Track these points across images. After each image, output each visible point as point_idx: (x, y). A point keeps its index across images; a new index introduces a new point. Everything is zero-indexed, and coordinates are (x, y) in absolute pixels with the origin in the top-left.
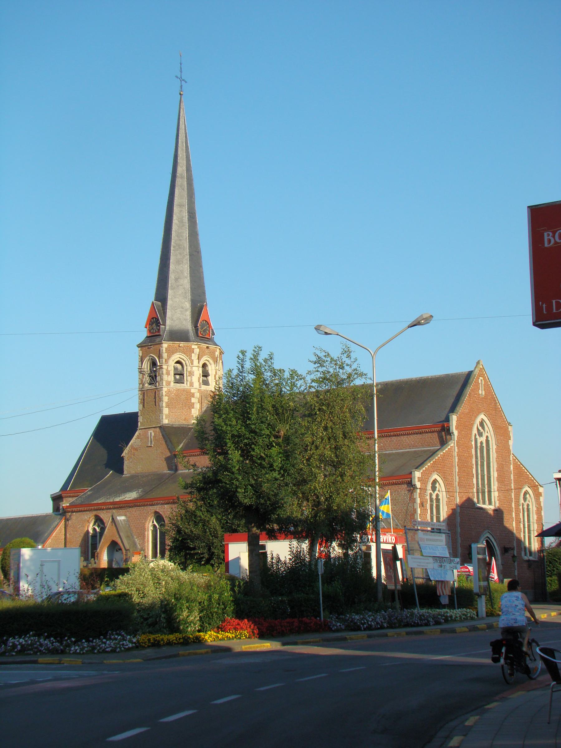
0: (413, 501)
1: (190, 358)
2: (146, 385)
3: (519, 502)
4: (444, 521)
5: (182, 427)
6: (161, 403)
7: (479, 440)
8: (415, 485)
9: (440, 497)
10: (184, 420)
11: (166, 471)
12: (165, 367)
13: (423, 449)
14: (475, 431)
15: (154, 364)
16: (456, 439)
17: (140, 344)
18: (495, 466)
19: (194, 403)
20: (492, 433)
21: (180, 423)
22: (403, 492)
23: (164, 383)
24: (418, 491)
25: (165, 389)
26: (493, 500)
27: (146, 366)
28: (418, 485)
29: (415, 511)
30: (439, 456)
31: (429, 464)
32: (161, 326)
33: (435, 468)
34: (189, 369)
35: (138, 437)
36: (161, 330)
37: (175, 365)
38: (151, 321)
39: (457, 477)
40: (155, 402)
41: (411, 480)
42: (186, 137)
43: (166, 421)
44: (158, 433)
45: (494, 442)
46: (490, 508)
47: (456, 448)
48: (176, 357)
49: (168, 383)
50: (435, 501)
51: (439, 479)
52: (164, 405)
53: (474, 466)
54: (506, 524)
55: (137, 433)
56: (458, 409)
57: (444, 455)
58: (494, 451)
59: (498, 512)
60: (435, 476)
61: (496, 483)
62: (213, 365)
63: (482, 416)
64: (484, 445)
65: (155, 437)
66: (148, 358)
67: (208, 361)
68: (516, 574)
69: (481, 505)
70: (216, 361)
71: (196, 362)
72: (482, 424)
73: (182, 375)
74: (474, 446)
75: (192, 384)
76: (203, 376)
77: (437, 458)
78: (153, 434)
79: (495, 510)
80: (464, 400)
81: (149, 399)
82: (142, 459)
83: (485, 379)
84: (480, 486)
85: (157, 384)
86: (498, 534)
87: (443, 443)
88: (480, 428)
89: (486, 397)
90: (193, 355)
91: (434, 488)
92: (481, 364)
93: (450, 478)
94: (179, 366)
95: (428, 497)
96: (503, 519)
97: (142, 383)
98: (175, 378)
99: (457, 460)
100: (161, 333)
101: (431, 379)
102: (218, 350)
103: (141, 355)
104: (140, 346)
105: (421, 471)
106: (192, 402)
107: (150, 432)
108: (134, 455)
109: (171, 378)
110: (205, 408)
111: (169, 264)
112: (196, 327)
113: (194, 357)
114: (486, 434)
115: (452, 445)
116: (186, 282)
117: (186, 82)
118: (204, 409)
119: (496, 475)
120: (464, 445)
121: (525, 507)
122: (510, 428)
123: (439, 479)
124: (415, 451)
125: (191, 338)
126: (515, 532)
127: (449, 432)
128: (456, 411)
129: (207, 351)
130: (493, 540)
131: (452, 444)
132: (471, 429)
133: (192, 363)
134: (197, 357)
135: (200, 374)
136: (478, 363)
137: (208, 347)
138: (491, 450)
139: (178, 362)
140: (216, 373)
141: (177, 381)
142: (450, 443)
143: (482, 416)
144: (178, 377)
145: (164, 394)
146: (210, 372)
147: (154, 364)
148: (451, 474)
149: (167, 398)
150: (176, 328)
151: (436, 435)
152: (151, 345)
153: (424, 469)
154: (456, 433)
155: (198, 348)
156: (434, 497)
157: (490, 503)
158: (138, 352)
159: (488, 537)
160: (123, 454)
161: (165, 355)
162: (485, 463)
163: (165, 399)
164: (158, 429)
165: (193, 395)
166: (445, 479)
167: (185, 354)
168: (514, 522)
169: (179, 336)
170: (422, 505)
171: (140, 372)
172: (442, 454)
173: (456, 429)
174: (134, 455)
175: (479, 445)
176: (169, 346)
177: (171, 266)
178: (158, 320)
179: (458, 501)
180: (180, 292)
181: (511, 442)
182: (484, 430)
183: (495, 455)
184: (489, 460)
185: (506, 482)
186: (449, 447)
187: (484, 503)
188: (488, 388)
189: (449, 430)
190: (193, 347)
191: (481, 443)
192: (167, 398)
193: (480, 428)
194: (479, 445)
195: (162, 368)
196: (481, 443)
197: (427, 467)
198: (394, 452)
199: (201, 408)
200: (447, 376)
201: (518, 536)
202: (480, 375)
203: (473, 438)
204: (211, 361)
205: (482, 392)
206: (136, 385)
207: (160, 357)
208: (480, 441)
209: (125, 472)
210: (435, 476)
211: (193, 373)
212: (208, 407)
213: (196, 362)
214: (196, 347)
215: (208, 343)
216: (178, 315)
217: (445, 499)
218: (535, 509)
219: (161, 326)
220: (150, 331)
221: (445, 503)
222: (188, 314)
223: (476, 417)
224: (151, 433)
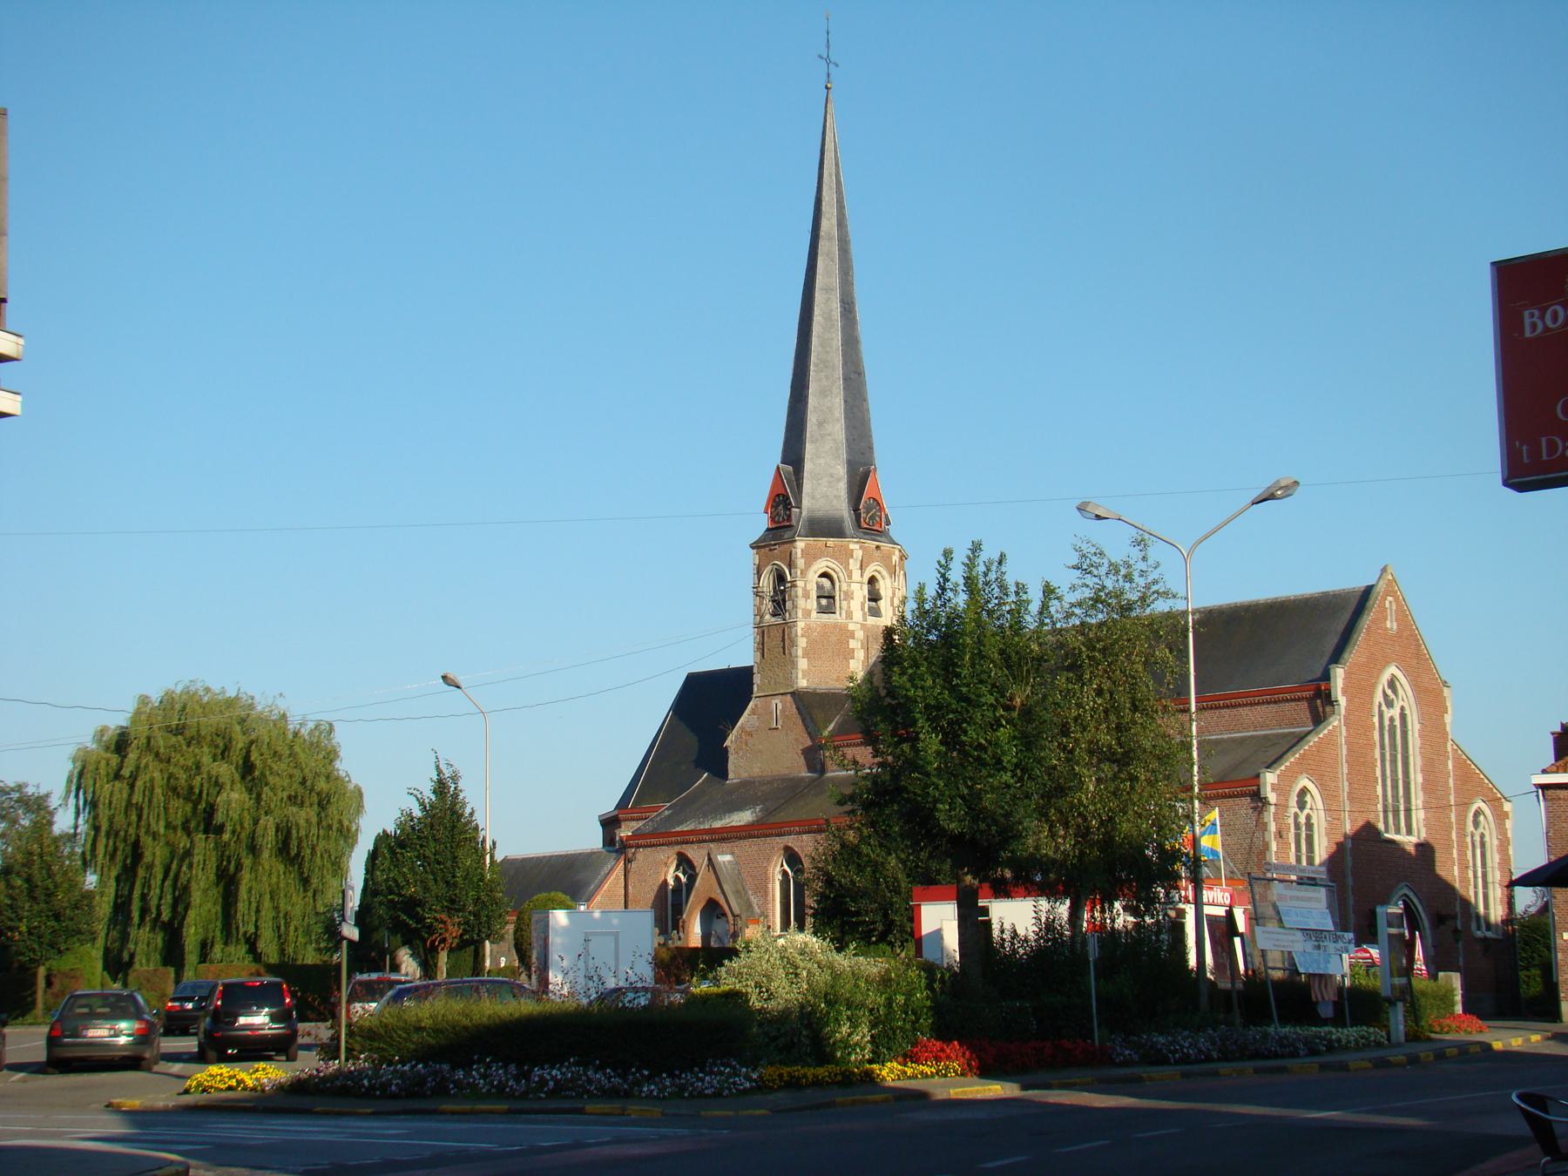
0: (1263, 827)
1: (847, 566)
2: (767, 617)
7: (1388, 713)
11: (805, 774)
14: (1379, 698)
15: (780, 578)
16: (1343, 712)
24: (1272, 809)
25: (801, 625)
28: (1272, 797)
29: (1266, 846)
34: (844, 587)
35: (753, 712)
43: (803, 683)
46: (1408, 841)
48: (821, 565)
49: (807, 613)
51: (1311, 786)
52: (800, 652)
54: (1441, 871)
56: (1346, 655)
59: (1426, 850)
60: (1305, 782)
61: (1421, 794)
62: (888, 580)
63: (1392, 670)
64: (1397, 723)
65: (783, 711)
71: (856, 575)
72: (1392, 684)
75: (849, 615)
81: (773, 642)
87: (1318, 719)
88: (1389, 692)
89: (1399, 635)
91: (1302, 805)
95: (1291, 821)
97: (759, 614)
99: (1345, 752)
100: (794, 522)
109: (812, 604)
112: (856, 510)
113: (854, 565)
118: (872, 660)
119: (1420, 779)
121: (1477, 838)
123: (1311, 786)
126: (1457, 885)
127: (1329, 700)
129: (877, 553)
131: (1336, 723)
133: (850, 577)
136: (1384, 570)
137: (878, 547)
139: (824, 575)
143: (1392, 670)
144: (824, 602)
146: (882, 593)
147: (780, 578)
148: (1335, 779)
150: (819, 514)
154: (1342, 701)
156: (1302, 820)
157: (1409, 832)
158: (752, 558)
161: (800, 562)
162: (1399, 757)
163: (802, 642)
166: (1323, 788)
169: (825, 528)
170: (1280, 834)
171: (756, 594)
173: (1344, 692)
175: (1386, 723)
179: (1348, 828)
180: (827, 447)
181: (1448, 718)
183: (1418, 742)
187: (1398, 831)
188: (1404, 616)
189: (1329, 695)
190: (852, 546)
191: (1392, 719)
193: (1389, 692)
194: (1386, 723)
196: (1392, 719)
200: (1325, 595)
202: (1387, 593)
204: (885, 573)
205: (1391, 624)
206: (749, 618)
207: (791, 566)
209: (731, 776)
210: (1305, 782)
213: (856, 575)
216: (824, 488)
217: (1324, 824)
218: (1496, 842)
220: (772, 519)
221: (1323, 831)
223: (1381, 671)
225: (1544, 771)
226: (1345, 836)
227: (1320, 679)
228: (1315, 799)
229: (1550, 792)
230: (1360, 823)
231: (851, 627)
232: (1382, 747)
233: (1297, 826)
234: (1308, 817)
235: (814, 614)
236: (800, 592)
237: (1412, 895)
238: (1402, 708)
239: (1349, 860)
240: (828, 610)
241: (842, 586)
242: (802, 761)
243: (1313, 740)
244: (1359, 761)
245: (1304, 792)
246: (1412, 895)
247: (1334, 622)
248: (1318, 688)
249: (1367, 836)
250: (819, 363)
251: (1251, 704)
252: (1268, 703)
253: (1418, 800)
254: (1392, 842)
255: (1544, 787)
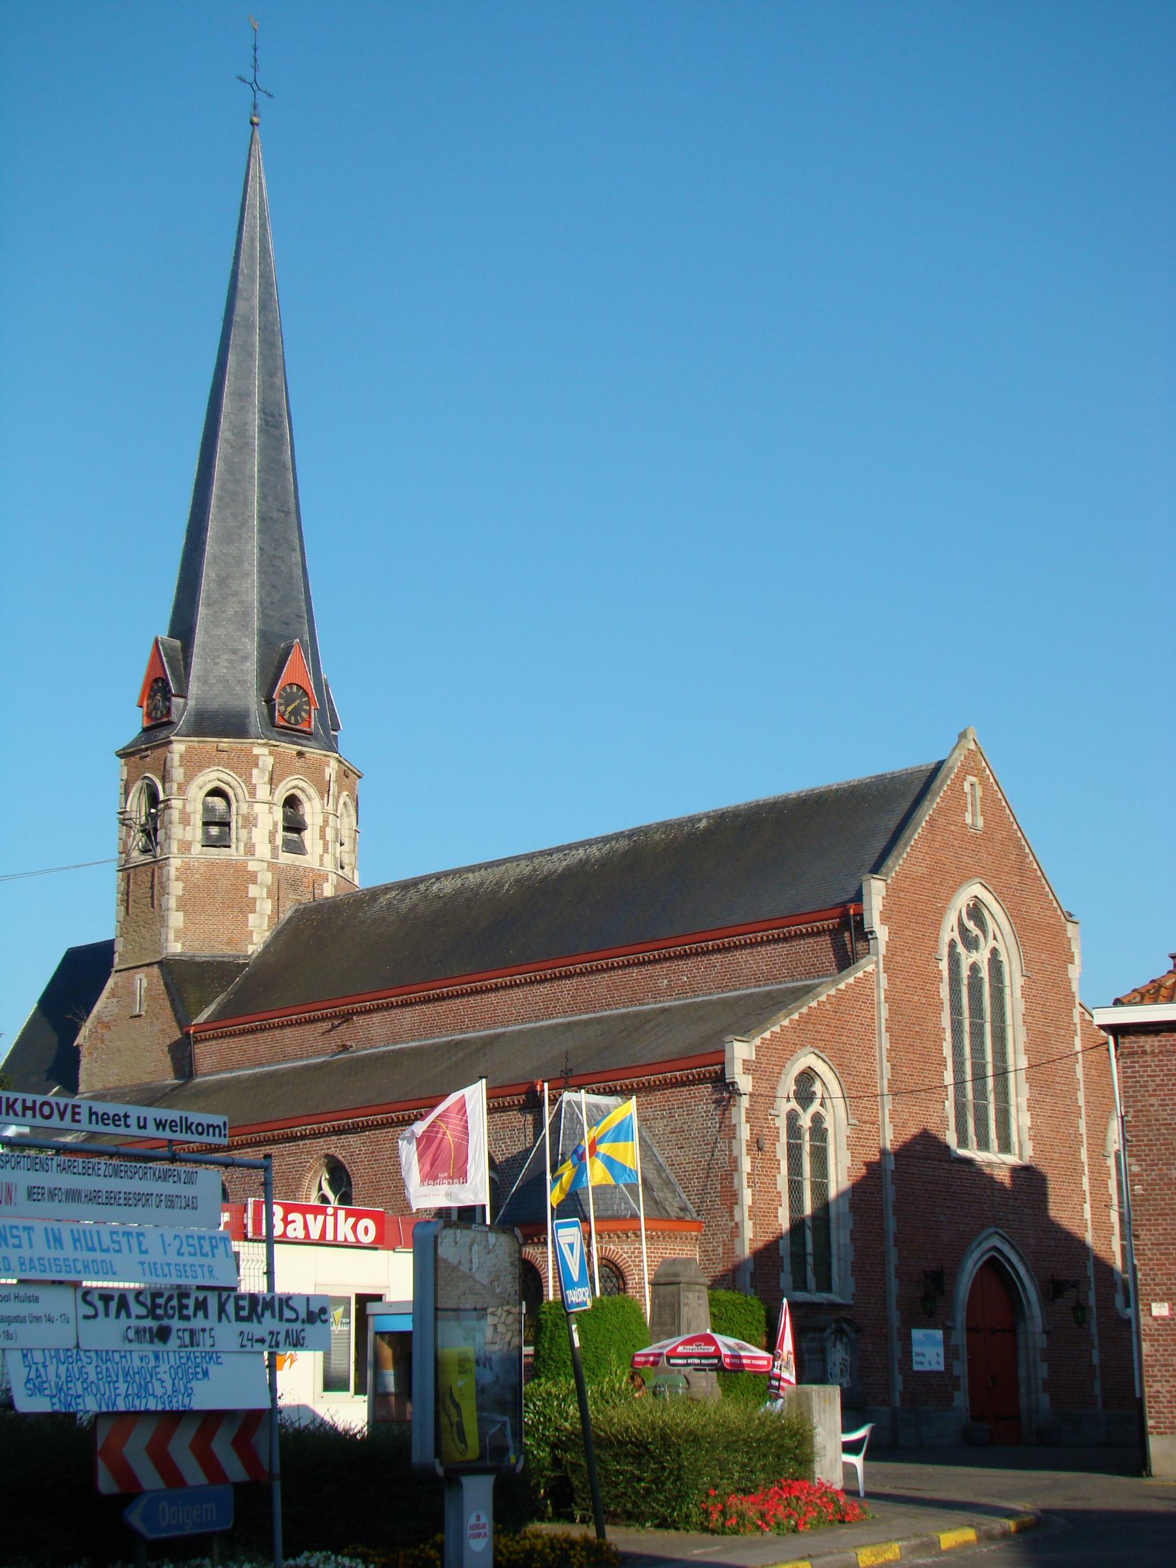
0: (729, 1131)
2: (135, 854)
3: (1104, 1146)
4: (841, 1195)
5: (219, 963)
6: (164, 900)
7: (967, 959)
8: (733, 1084)
9: (828, 1124)
10: (228, 944)
11: (171, 1081)
12: (176, 804)
13: (790, 985)
14: (949, 932)
15: (153, 799)
16: (882, 950)
17: (123, 749)
18: (1022, 1038)
19: (254, 899)
20: (1010, 939)
21: (216, 952)
22: (702, 1108)
23: (174, 847)
24: (745, 1102)
25: (175, 863)
26: (1014, 1138)
27: (137, 805)
28: (745, 1083)
29: (735, 1163)
30: (823, 998)
31: (786, 1023)
32: (174, 699)
33: (804, 1035)
34: (244, 809)
35: (113, 994)
36: (173, 709)
37: (210, 799)
38: (152, 687)
39: (887, 1066)
40: (152, 897)
41: (723, 1070)
42: (263, 226)
43: (175, 948)
44: (155, 981)
45: (1016, 966)
46: (997, 1162)
47: (883, 977)
48: (210, 777)
49: (186, 846)
50: (807, 1137)
51: (821, 1067)
52: (173, 903)
53: (948, 1035)
54: (1058, 1212)
55: (110, 983)
56: (889, 862)
57: (841, 994)
58: (1018, 993)
59: (1029, 1179)
60: (807, 1059)
61: (1025, 1088)
62: (317, 802)
63: (975, 889)
64: (985, 974)
65: (148, 990)
66: (139, 784)
67: (301, 789)
68: (1096, 1360)
69: (961, 1152)
70: (324, 790)
71: (263, 792)
72: (976, 911)
73: (225, 824)
74: (946, 974)
75: (250, 849)
76: (286, 829)
77: (814, 1004)
78: (145, 984)
79: (1018, 1172)
80: (910, 838)
81: (140, 891)
82: (119, 1050)
83: (983, 781)
84: (970, 1095)
85: (158, 849)
86: (1032, 1241)
87: (845, 961)
88: (970, 925)
89: (987, 835)
90: (255, 771)
91: (804, 1096)
92: (970, 737)
93: (862, 1067)
94: (218, 802)
95: (782, 1123)
96: (1045, 1194)
97: (126, 851)
98: (206, 834)
99: (884, 1013)
100: (174, 717)
101: (837, 790)
102: (334, 764)
103: (125, 777)
104: (124, 755)
105: (758, 1041)
106: (251, 895)
107: (138, 976)
108: (102, 1041)
109: (196, 832)
110: (289, 914)
111: (204, 543)
112: (269, 701)
113: (259, 777)
114: (992, 943)
115: (870, 968)
116: (251, 590)
117: (270, 96)
118: (285, 916)
120: (909, 970)
122: (1071, 929)
123: (821, 1067)
124: (769, 993)
125: (252, 730)
126: (1089, 1238)
127: (864, 935)
128: (884, 870)
129: (299, 763)
130: (1014, 1258)
131: (869, 966)
132: (937, 925)
133: (253, 793)
134: (267, 778)
135: (275, 824)
136: (963, 735)
137: (300, 754)
138: (1007, 991)
139: (216, 792)
140: (326, 822)
141: (210, 842)
142: (863, 961)
143: (975, 889)
144: (214, 831)
145: (173, 873)
146: (308, 819)
147: (153, 799)
148: (868, 1054)
149: (181, 885)
150: (214, 705)
151: (825, 942)
152: (147, 749)
153: (767, 1035)
154: (882, 933)
155: (271, 753)
156: (805, 1121)
157: (1005, 1147)
158: (119, 769)
159: (995, 1248)
160: (79, 1040)
161: (178, 773)
162: (988, 1027)
163: (176, 889)
164: (156, 970)
165: (253, 878)
166: (842, 1069)
167: (232, 769)
168: (1087, 1207)
169: (222, 724)
170: (757, 1145)
171: (123, 823)
172: (833, 992)
173: (885, 919)
174: (102, 1041)
175: (965, 972)
176: (189, 750)
177: (207, 548)
178: (168, 684)
179: (889, 1138)
180: (230, 612)
181: (1074, 972)
182: (984, 931)
183: (1021, 1006)
184: (1003, 1021)
185: (1058, 1087)
186: (860, 974)
187: (983, 1144)
188: (994, 806)
189: (860, 924)
190: (257, 751)
191: (974, 968)
192: (181, 885)
193: (970, 925)
194: (965, 972)
195: (168, 807)
196: (974, 968)
197: (776, 1029)
198: (715, 997)
199: (277, 911)
200: (880, 778)
201: (1102, 1254)
202: (965, 771)
203: (944, 951)
204: (311, 791)
205: (975, 819)
206: (112, 851)
207: (165, 778)
208: (970, 961)
209: (82, 1088)
210: (807, 1059)
211: (256, 818)
212: (296, 911)
213: (263, 792)
214: (265, 751)
215: (305, 742)
216: (225, 666)
217: (845, 1131)
219: (174, 699)
220: (149, 715)
221: (843, 1142)
222: (251, 667)
223: (954, 889)
224: (142, 980)
225: (1118, 1002)
226: (883, 1152)
227: (851, 901)
228: (829, 1081)
229: (1127, 1041)
230: (913, 1130)
231: (252, 866)
232: (956, 1009)
233: (794, 1130)
234: (817, 1119)
235: (197, 848)
236: (175, 815)
237: (1006, 1249)
238: (994, 952)
239: (890, 1191)
240: (221, 842)
241: (240, 808)
242: (167, 1061)
243: (827, 993)
244: (910, 1031)
245: (807, 1077)
246: (1006, 1249)
247: (875, 816)
248: (845, 916)
249: (924, 1151)
250: (239, 495)
251: (753, 945)
252: (776, 941)
253: (1020, 1094)
254: (969, 1162)
255: (1118, 1031)
